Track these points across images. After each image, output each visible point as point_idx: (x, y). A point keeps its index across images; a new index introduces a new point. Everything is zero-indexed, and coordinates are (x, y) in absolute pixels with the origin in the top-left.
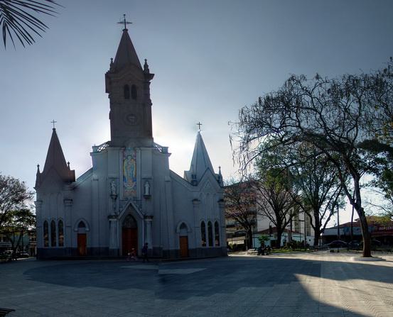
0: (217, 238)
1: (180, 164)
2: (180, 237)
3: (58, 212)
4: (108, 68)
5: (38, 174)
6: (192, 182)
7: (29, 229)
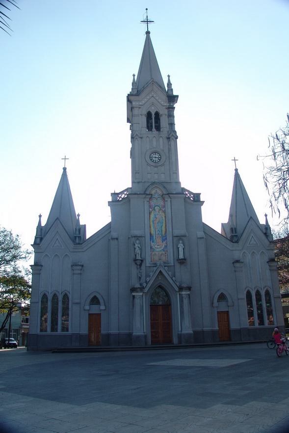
0: (270, 313)
1: (216, 215)
2: (218, 312)
3: (61, 281)
4: (129, 89)
5: (40, 228)
6: (232, 237)
7: (23, 305)
